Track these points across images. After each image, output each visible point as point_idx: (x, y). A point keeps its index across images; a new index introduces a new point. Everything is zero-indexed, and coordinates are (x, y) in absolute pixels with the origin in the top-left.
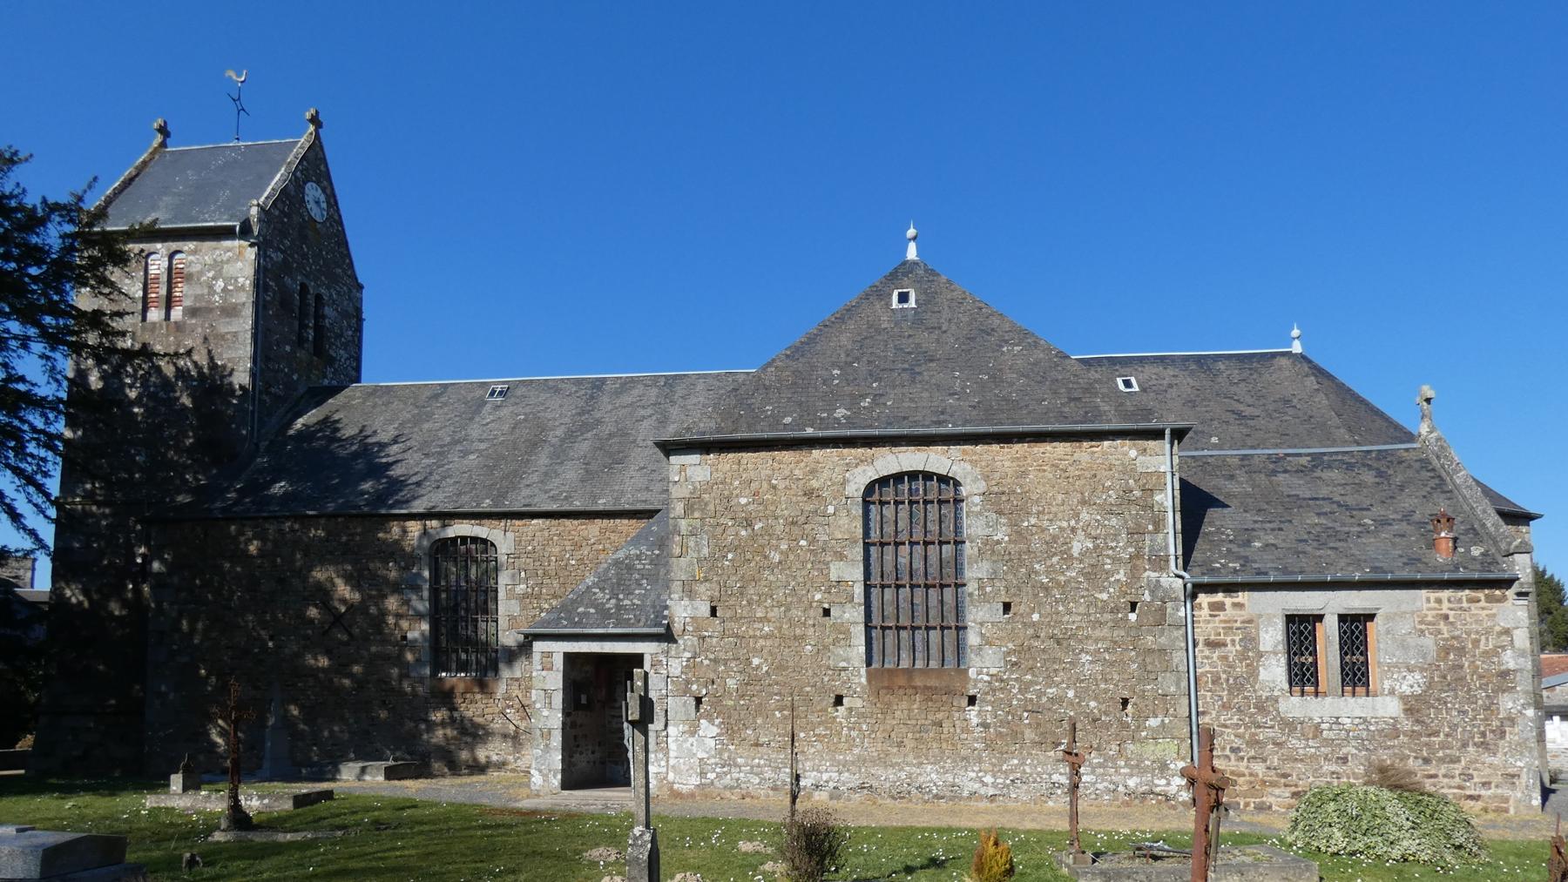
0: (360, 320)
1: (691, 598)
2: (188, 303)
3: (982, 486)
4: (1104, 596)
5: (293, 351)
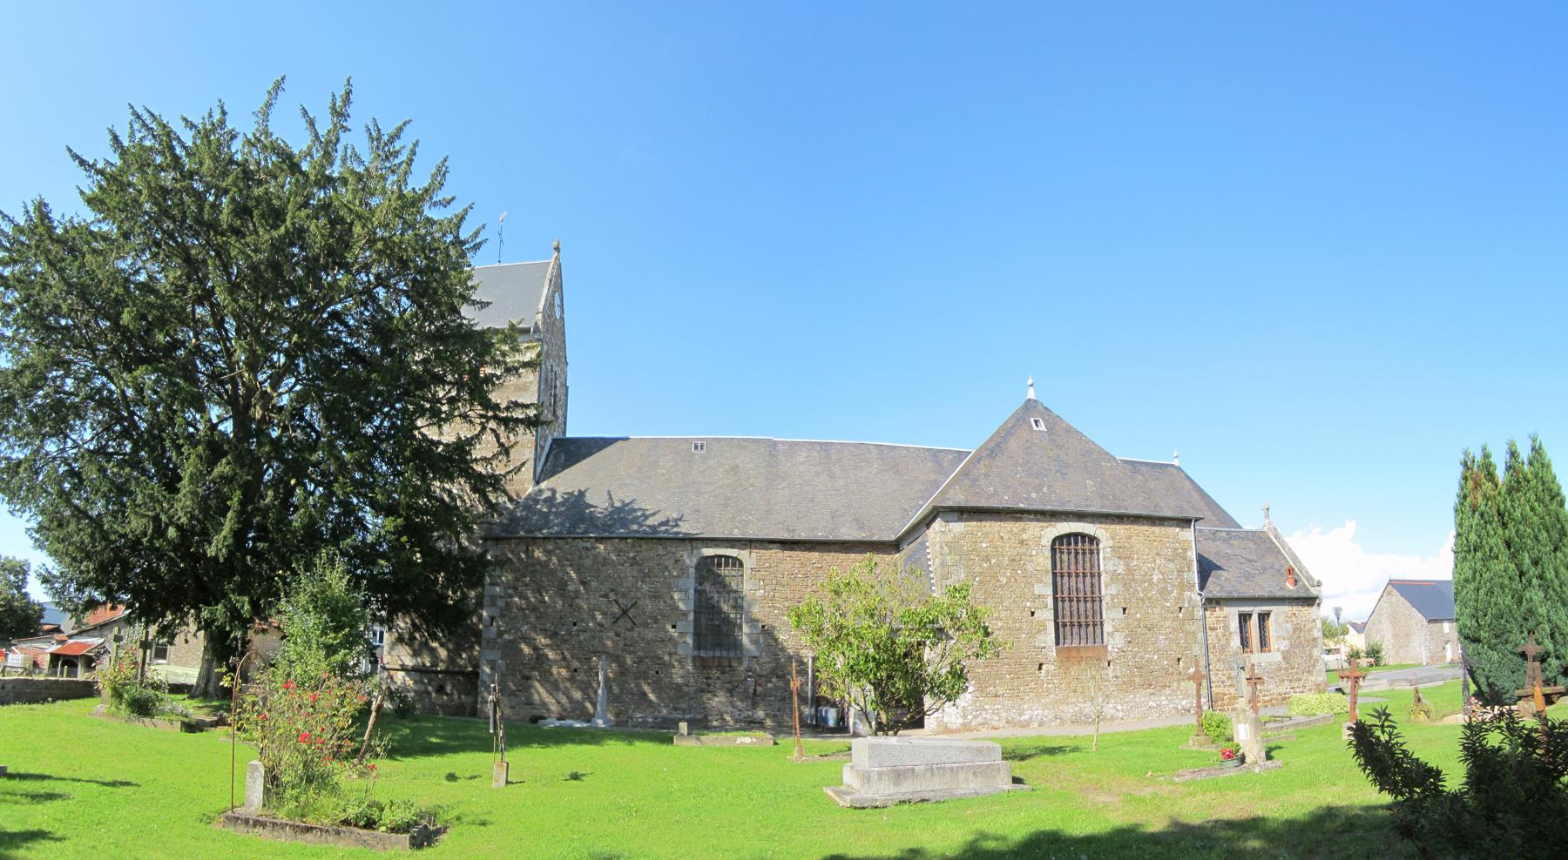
3: (1111, 543)
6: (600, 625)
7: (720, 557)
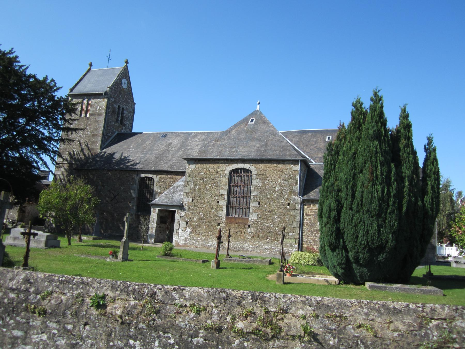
0: (134, 113)
1: (188, 197)
2: (91, 112)
3: (256, 172)
4: (282, 201)
5: (115, 124)
6: (107, 201)
7: (147, 177)
